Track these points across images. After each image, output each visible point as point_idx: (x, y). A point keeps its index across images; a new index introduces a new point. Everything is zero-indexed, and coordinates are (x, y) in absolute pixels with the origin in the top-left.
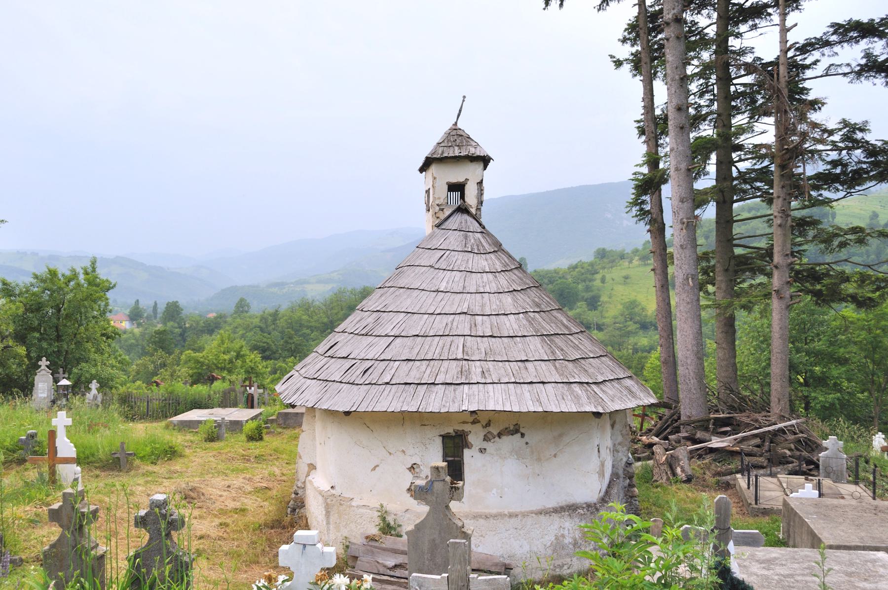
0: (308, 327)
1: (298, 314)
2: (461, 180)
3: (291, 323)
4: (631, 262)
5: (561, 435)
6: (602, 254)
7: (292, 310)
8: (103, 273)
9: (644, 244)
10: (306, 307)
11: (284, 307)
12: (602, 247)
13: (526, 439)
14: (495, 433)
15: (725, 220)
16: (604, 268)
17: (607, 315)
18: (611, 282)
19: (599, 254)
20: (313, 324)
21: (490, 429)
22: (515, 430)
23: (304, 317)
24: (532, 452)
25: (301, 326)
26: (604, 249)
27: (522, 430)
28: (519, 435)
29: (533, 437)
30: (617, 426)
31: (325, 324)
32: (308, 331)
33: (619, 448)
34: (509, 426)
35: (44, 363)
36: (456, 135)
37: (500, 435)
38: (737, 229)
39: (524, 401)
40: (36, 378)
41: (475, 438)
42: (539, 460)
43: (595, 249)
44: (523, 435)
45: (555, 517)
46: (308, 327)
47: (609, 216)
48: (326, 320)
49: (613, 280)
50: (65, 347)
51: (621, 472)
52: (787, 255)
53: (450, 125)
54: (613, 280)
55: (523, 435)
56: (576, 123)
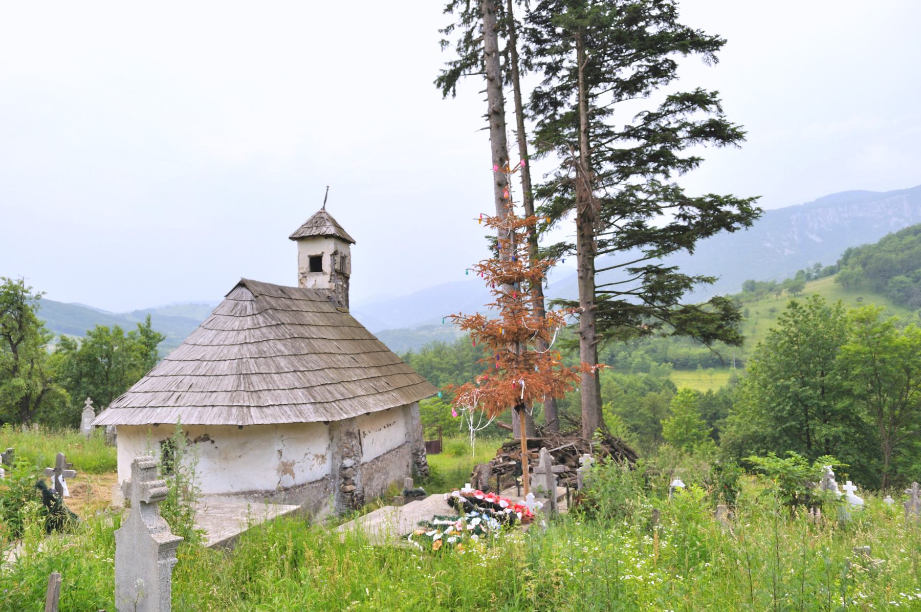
0: (438, 369)
1: (430, 356)
2: (319, 253)
3: (423, 366)
4: (779, 293)
5: (245, 443)
6: (751, 287)
7: (424, 352)
8: (155, 328)
9: (798, 274)
10: (440, 351)
11: (416, 351)
12: (751, 279)
13: (216, 444)
14: (192, 440)
15: (587, 271)
16: (750, 301)
17: (748, 351)
18: (756, 315)
19: (747, 286)
20: (444, 366)
21: (189, 437)
22: (206, 438)
23: (434, 359)
24: (220, 454)
25: (432, 368)
26: (753, 282)
27: (212, 438)
28: (209, 442)
29: (221, 444)
30: (335, 440)
31: (456, 366)
32: (438, 373)
33: (336, 456)
34: (202, 435)
35: (89, 402)
36: (321, 218)
37: (195, 442)
38: (599, 279)
39: (212, 418)
40: (83, 414)
41: (182, 444)
42: (226, 459)
43: (744, 281)
44: (213, 442)
45: (234, 498)
46: (438, 369)
47: (769, 245)
48: (456, 362)
49: (758, 313)
50: (109, 389)
51: (337, 474)
52: (589, 303)
53: (319, 209)
54: (758, 313)
55: (213, 442)
56: (426, 199)
